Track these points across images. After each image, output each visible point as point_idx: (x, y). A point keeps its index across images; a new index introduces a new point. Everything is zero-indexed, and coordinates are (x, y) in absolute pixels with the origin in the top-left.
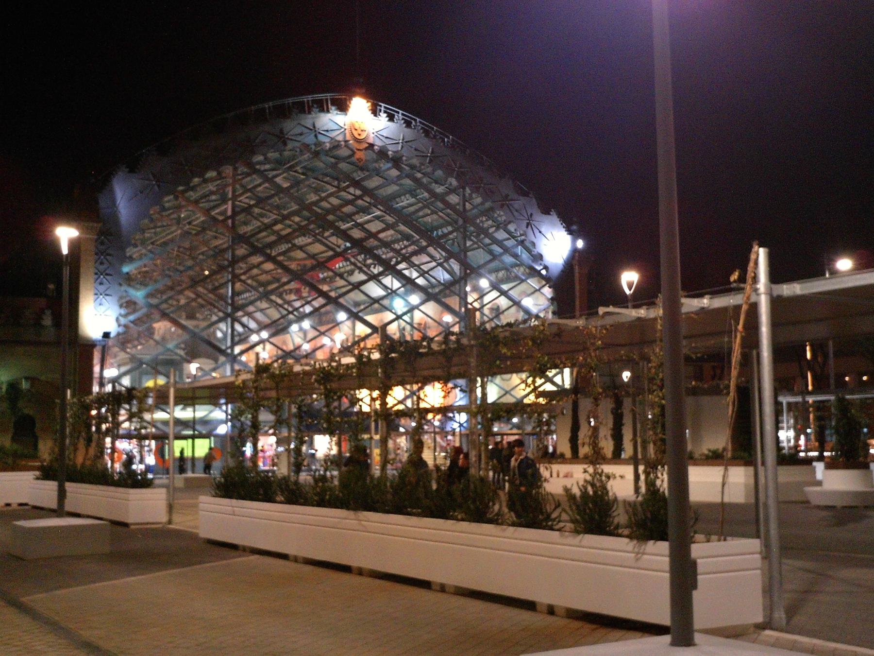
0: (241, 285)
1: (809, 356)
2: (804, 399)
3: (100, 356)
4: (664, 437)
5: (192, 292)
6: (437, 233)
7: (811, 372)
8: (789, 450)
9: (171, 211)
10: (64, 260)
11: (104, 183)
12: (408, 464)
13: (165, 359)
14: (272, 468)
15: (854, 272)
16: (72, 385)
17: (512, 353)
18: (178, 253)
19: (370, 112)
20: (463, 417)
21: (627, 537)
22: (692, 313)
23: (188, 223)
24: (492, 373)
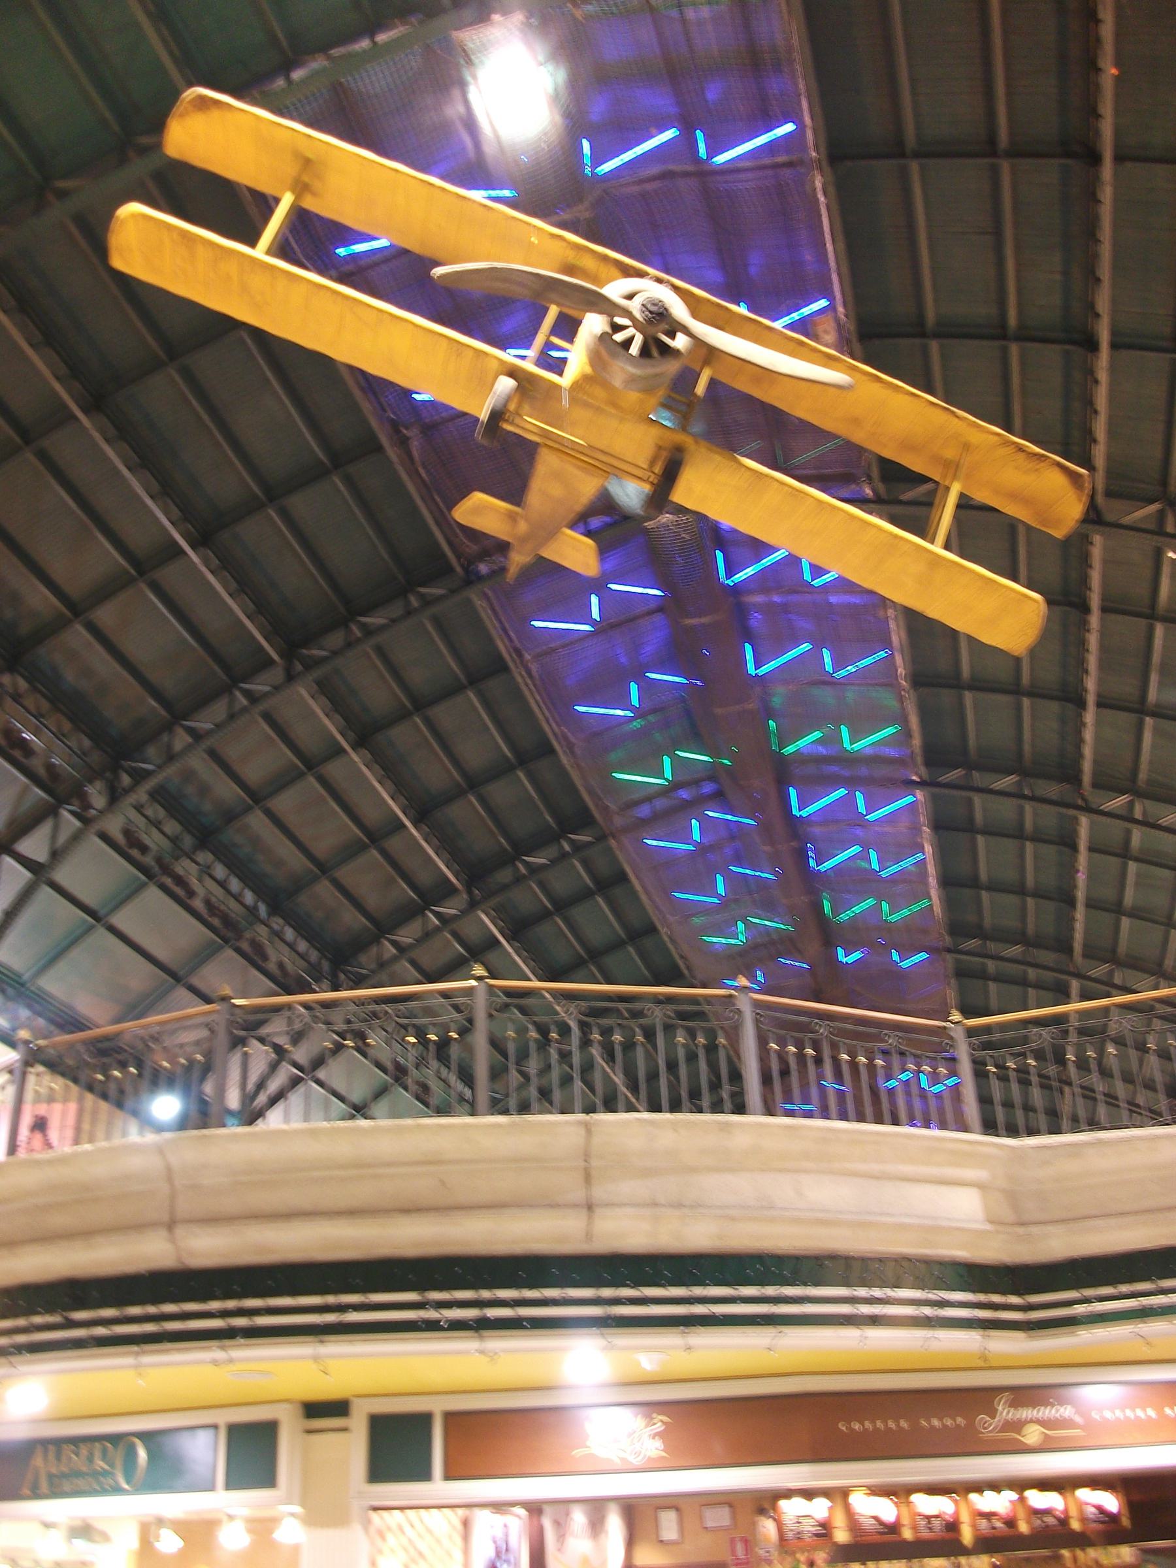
1: (586, 145)
4: (37, 1088)
7: (678, 750)
12: (539, 1053)
13: (146, 1018)
14: (1129, 1413)
16: (725, 1095)
17: (928, 1421)
18: (946, 1096)
20: (882, 1428)
22: (471, 1320)
23: (555, 331)
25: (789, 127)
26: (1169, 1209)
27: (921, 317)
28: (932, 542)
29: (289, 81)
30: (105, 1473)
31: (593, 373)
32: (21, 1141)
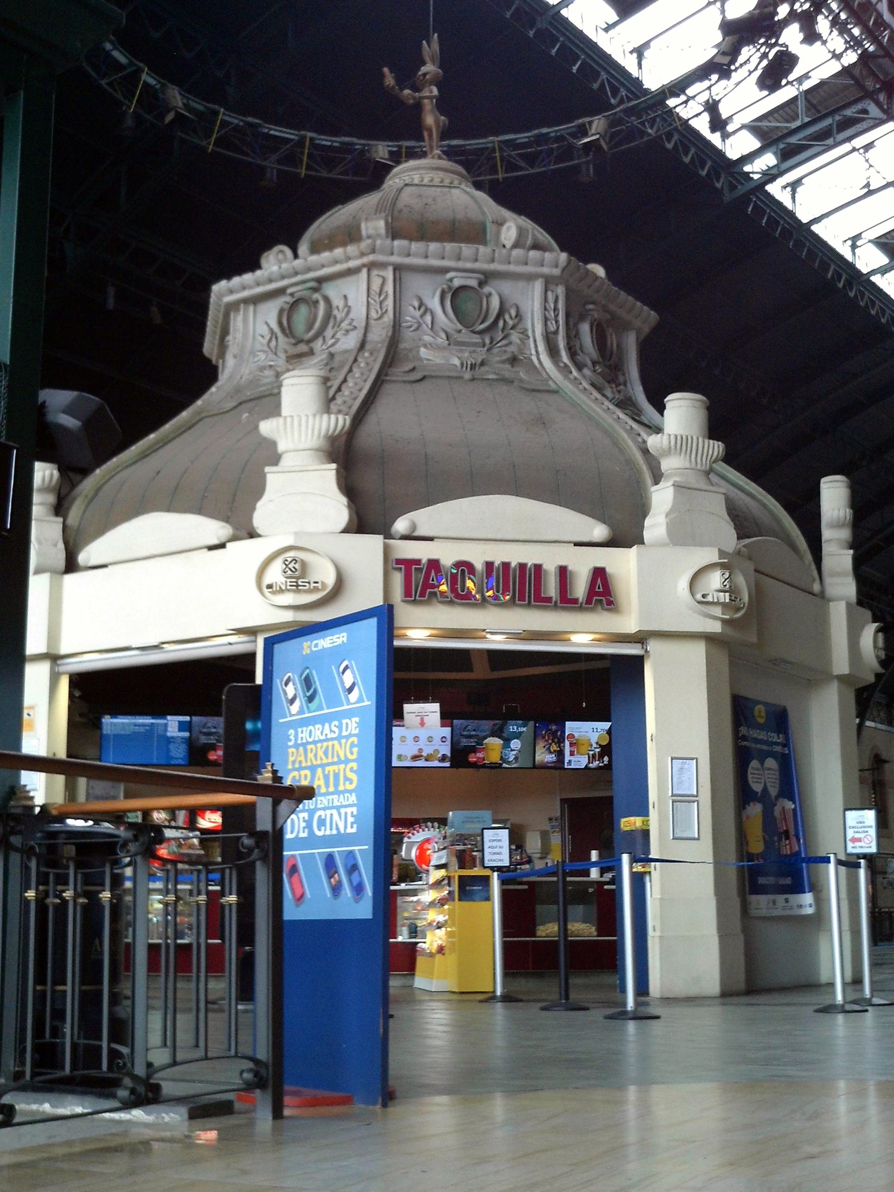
3: (200, 918)
9: (525, 879)
19: (774, 183)
25: (219, 941)
26: (893, 854)
27: (494, 992)
28: (286, 718)
29: (129, 879)
30: (679, 132)
31: (124, 887)
32: (869, 104)
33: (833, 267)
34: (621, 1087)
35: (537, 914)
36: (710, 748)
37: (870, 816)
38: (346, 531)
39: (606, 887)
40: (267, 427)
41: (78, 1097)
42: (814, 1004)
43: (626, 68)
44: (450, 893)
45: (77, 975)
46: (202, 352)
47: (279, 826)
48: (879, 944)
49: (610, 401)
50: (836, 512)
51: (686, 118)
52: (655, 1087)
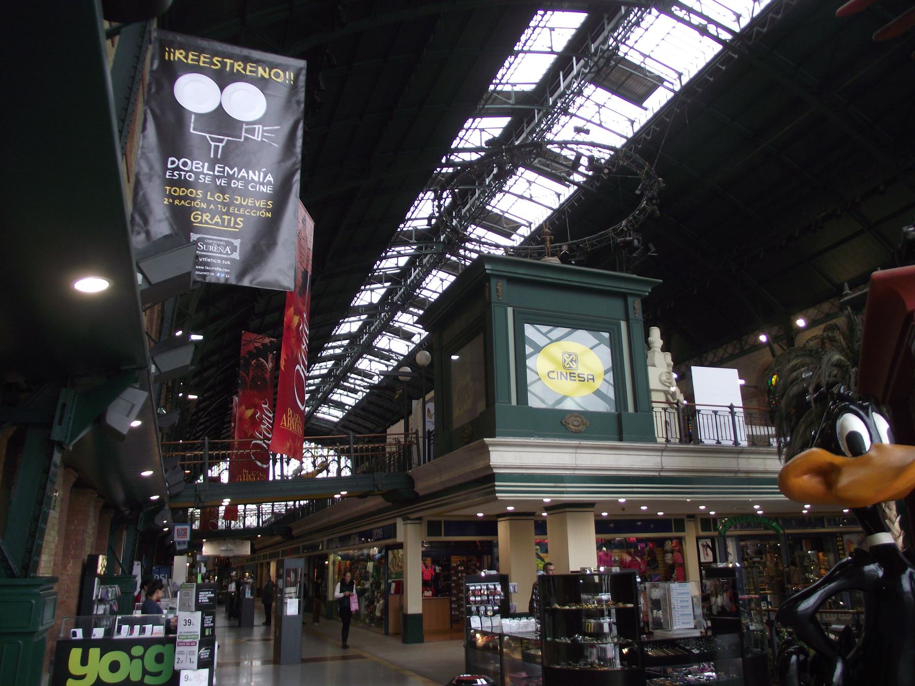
0: (301, 69)
2: (784, 531)
5: (150, 80)
6: (785, 439)
8: (517, 103)
10: (624, 543)
11: (272, 481)
15: (887, 529)
19: (614, 146)
21: (703, 613)
24: (661, 570)
32: (701, 632)
33: (717, 64)
34: (494, 474)
35: (497, 408)
36: (495, 421)
37: (740, 659)
38: (98, 677)
39: (219, 157)
40: (742, 382)
41: (907, 494)
42: (308, 584)
43: (561, 12)
44: (486, 103)
45: (487, 486)
46: (68, 670)
47: (124, 157)
48: (232, 618)
49: (165, 598)
50: (589, 86)
51: (602, 345)
52: (491, 463)
